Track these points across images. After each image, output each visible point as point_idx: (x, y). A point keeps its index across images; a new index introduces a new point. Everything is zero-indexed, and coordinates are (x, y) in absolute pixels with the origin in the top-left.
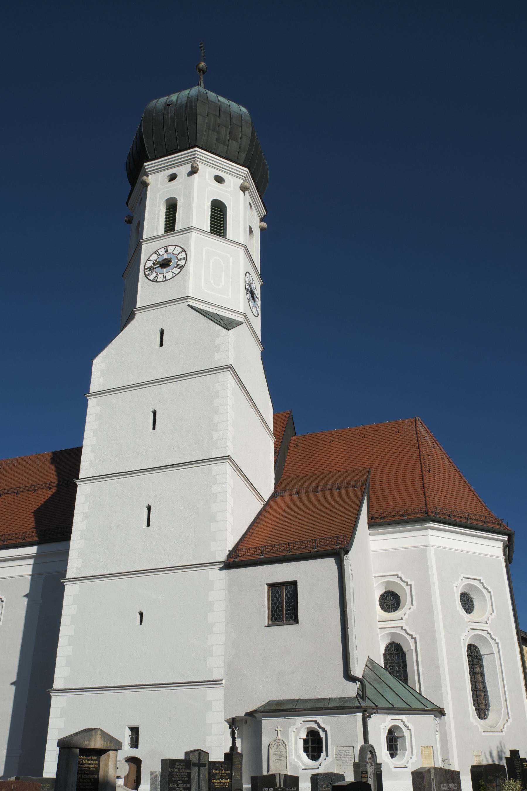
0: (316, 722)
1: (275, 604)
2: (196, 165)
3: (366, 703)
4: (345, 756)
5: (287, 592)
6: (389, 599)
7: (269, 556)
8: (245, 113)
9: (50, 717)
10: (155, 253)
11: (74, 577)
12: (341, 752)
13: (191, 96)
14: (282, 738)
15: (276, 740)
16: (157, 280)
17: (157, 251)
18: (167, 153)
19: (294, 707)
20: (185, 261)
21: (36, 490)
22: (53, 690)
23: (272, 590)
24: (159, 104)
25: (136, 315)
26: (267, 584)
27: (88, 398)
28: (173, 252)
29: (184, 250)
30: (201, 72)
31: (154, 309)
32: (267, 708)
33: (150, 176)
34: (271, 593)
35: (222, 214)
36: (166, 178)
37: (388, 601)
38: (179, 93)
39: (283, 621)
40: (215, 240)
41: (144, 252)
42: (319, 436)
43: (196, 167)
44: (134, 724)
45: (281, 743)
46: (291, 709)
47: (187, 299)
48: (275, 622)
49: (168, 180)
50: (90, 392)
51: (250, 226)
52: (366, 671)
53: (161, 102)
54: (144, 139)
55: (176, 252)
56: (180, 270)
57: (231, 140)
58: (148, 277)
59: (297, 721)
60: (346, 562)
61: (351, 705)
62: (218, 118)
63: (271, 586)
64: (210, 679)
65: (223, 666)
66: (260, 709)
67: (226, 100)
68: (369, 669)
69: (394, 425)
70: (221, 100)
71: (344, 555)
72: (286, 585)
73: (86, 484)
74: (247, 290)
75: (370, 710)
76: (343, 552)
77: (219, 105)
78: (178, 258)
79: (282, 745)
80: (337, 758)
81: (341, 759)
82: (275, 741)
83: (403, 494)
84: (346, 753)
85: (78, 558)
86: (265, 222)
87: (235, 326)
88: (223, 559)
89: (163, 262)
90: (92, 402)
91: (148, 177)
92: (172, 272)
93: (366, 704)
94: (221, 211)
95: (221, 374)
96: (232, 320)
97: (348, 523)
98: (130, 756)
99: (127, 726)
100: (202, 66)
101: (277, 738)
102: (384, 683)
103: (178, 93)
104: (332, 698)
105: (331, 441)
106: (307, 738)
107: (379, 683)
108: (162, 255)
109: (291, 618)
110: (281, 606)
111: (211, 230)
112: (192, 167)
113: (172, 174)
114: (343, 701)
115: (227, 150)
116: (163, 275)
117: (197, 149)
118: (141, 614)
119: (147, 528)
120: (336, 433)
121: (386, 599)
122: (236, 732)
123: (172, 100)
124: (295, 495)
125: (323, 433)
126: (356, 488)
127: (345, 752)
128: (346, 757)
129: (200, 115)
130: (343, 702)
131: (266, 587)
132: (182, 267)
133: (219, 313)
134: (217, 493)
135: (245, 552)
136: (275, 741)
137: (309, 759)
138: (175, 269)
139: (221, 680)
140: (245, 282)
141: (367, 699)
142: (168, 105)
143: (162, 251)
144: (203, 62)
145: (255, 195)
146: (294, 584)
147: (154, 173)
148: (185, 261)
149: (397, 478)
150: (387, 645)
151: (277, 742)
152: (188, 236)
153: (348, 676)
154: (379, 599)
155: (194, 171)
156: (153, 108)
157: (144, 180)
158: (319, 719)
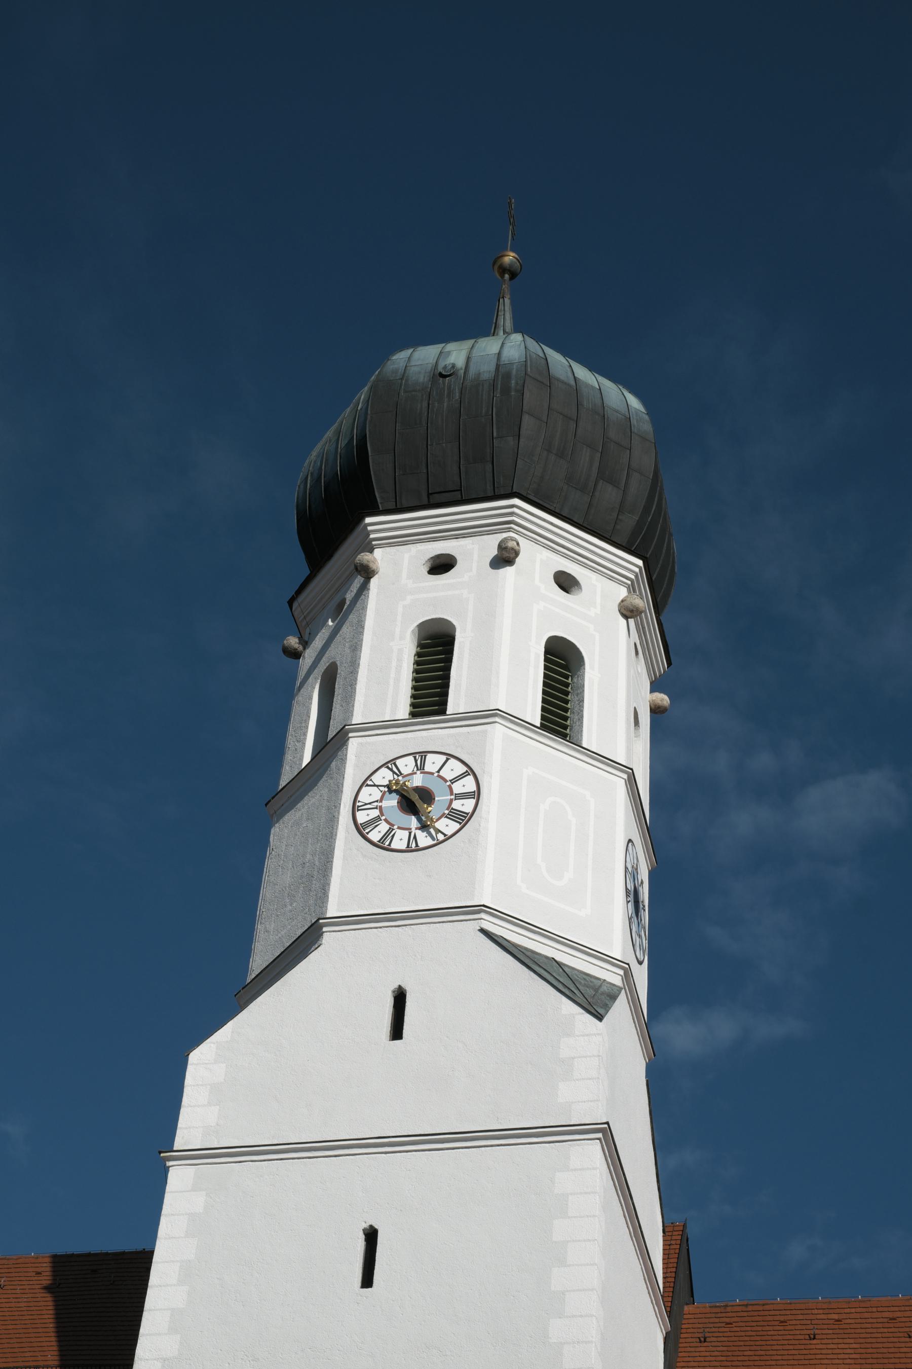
2: (515, 544)
8: (637, 411)
10: (388, 767)
17: (393, 761)
20: (473, 801)
27: (169, 1163)
28: (438, 771)
29: (470, 771)
30: (507, 276)
31: (380, 928)
33: (376, 551)
35: (570, 674)
42: (771, 1313)
43: (513, 549)
50: (175, 1149)
51: (635, 708)
54: (370, 454)
55: (447, 773)
56: (458, 826)
62: (572, 425)
74: (627, 891)
77: (576, 389)
78: (456, 791)
86: (665, 693)
91: (371, 551)
94: (566, 667)
100: (511, 260)
105: (812, 1336)
111: (541, 724)
112: (502, 547)
115: (590, 504)
116: (410, 833)
117: (516, 501)
120: (821, 1311)
123: (453, 366)
132: (463, 820)
138: (444, 821)
140: (626, 868)
143: (407, 765)
144: (513, 250)
148: (473, 801)
149: (779, 1353)
152: (485, 732)
157: (365, 562)
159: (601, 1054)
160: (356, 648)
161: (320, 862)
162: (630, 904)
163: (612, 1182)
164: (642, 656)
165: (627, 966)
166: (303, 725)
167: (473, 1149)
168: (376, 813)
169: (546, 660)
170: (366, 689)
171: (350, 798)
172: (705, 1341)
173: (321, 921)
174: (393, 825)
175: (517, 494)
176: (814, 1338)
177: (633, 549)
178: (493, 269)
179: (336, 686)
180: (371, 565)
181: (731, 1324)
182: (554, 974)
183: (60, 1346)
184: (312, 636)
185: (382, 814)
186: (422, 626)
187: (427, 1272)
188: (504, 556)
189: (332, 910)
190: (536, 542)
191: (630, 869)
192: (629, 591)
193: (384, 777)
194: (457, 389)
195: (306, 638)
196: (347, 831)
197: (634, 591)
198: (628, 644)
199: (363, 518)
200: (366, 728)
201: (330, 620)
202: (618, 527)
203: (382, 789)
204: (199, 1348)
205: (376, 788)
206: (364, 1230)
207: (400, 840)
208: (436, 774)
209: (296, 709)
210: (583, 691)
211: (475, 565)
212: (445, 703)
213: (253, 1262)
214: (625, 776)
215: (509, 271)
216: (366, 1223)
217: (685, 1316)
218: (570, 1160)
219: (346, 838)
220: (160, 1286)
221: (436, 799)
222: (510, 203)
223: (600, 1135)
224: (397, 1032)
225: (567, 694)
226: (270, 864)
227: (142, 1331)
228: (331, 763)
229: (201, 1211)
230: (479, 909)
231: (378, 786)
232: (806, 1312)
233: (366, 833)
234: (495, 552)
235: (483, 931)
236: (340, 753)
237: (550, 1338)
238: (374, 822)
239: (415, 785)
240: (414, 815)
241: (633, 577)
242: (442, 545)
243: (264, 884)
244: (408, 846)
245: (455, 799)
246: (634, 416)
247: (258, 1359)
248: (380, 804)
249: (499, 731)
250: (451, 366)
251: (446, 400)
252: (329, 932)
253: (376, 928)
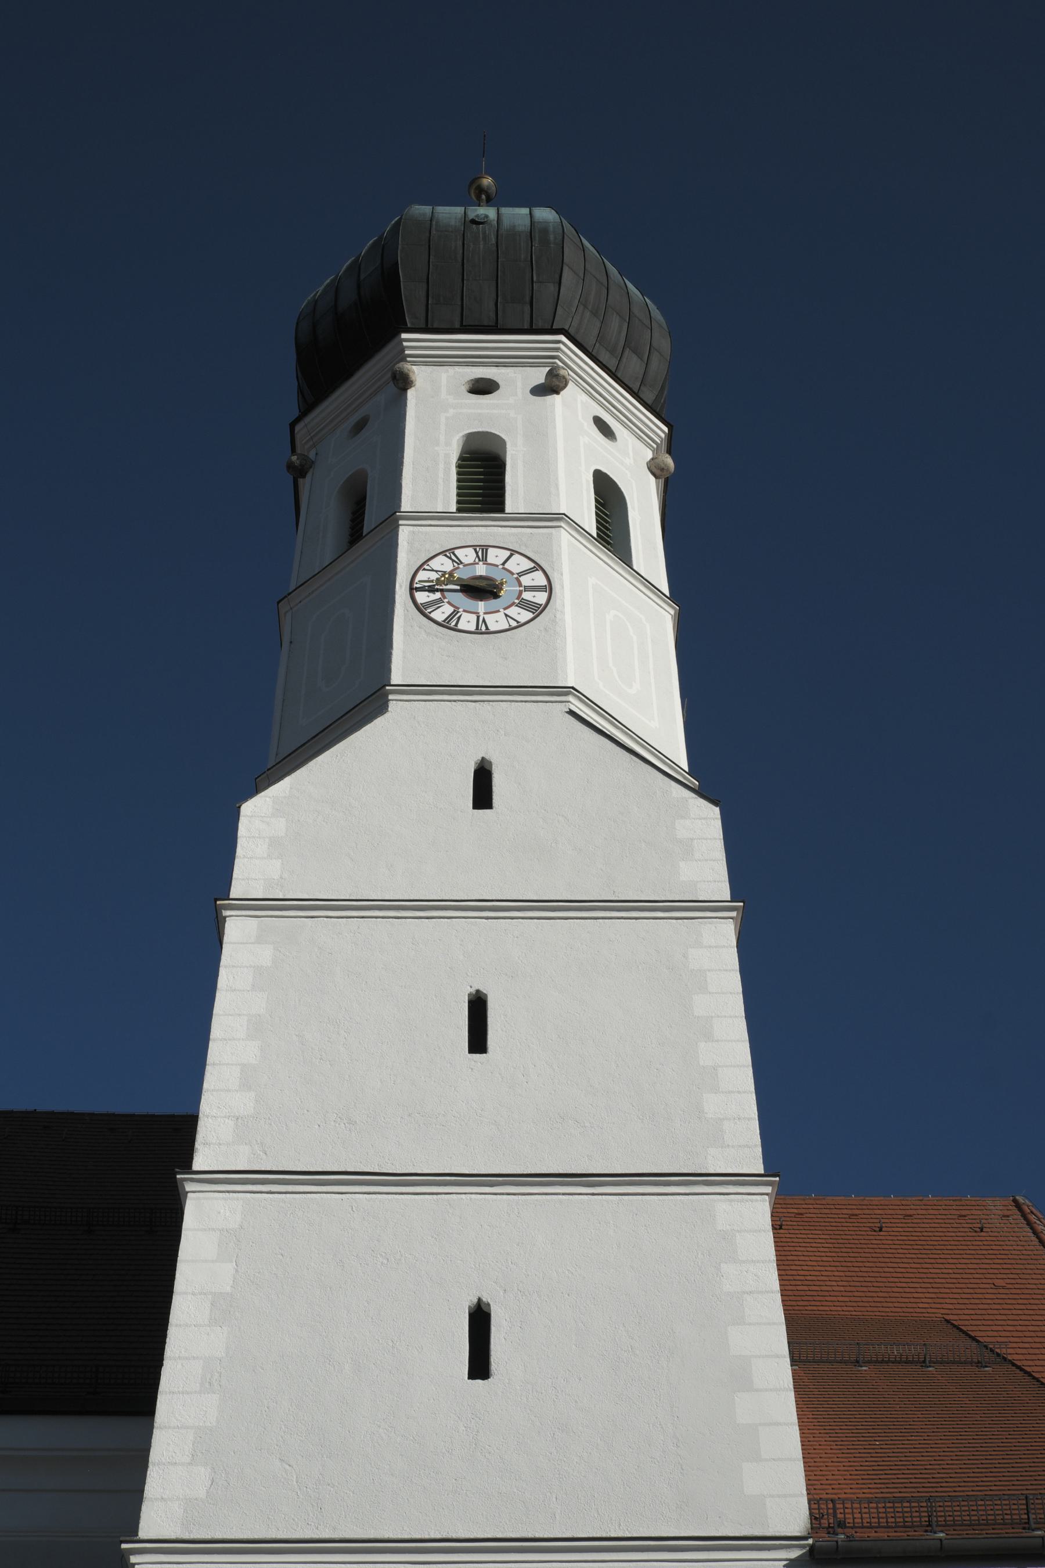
10: (475, 550)
16: (430, 613)
25: (391, 704)
27: (226, 913)
31: (455, 701)
36: (464, 383)
41: (405, 543)
50: (231, 896)
56: (530, 615)
78: (524, 583)
85: (190, 1464)
88: (797, 1528)
89: (472, 583)
92: (506, 615)
134: (744, 1293)
143: (467, 556)
155: (552, 386)
167: (589, 920)
170: (412, 485)
171: (407, 580)
174: (458, 608)
175: (564, 331)
178: (469, 193)
180: (411, 374)
186: (470, 438)
187: (552, 1040)
188: (553, 384)
200: (417, 516)
204: (280, 1107)
208: (501, 567)
213: (338, 1020)
214: (672, 612)
216: (471, 987)
218: (702, 937)
220: (225, 1040)
229: (269, 965)
230: (567, 691)
233: (429, 612)
235: (571, 713)
237: (706, 1113)
242: (481, 370)
245: (525, 591)
247: (356, 1122)
249: (564, 537)
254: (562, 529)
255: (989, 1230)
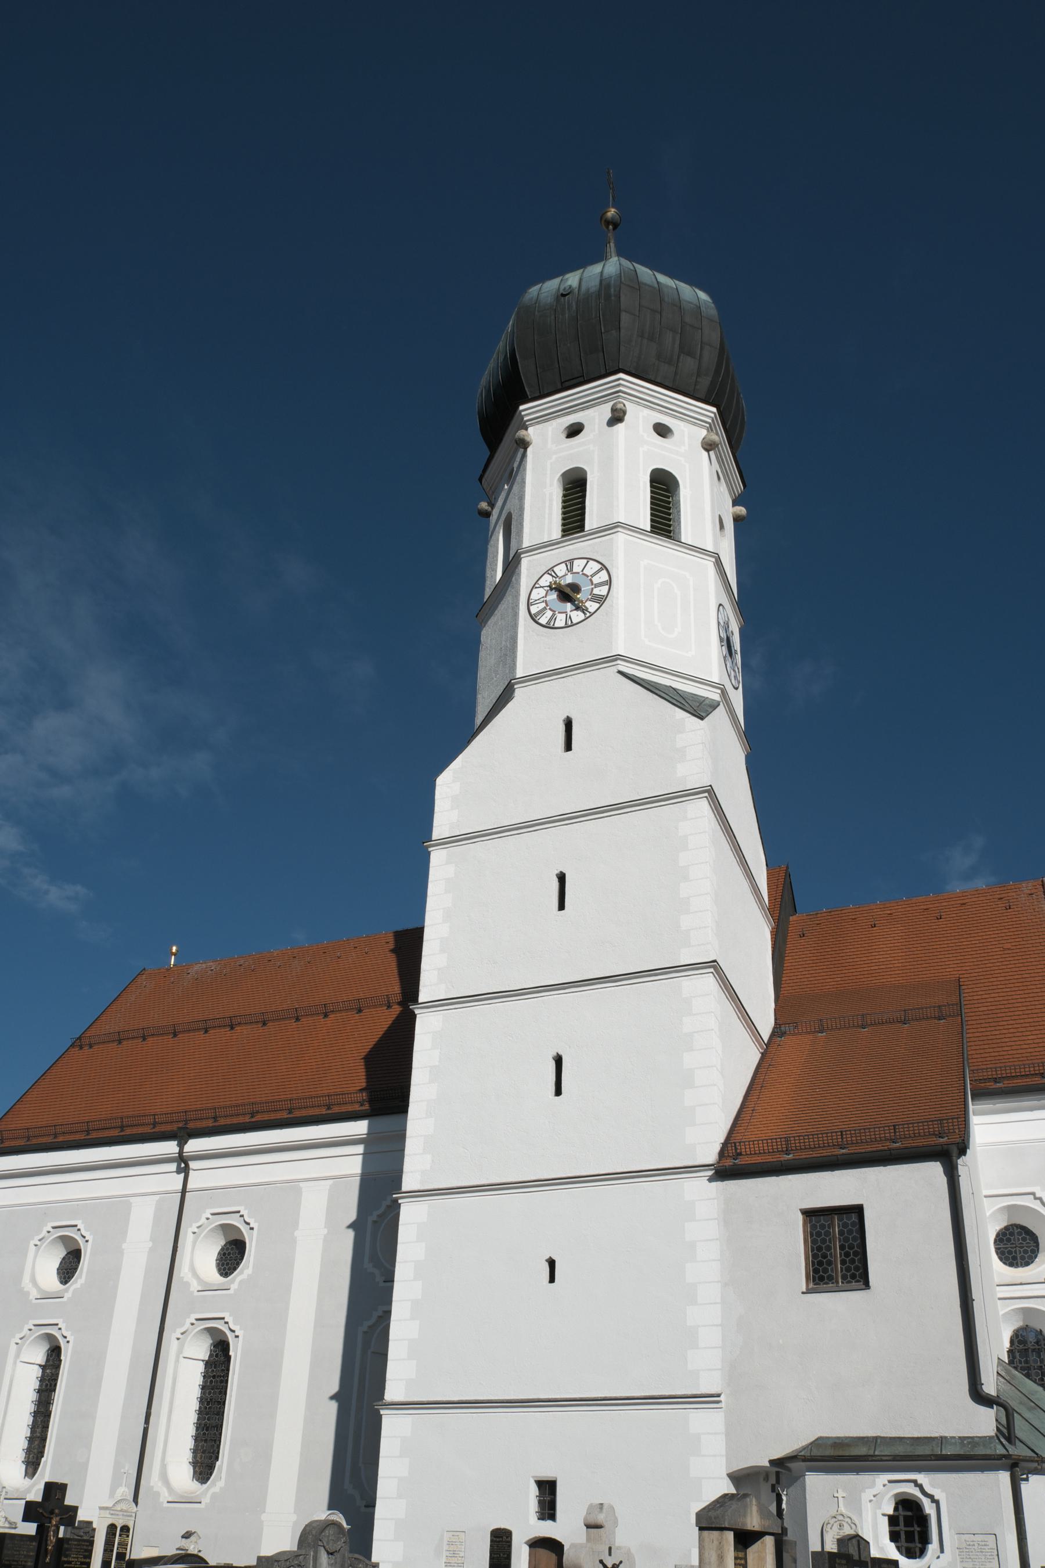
0: (915, 1482)
1: (819, 1249)
2: (622, 405)
3: (1016, 1448)
4: (978, 1552)
5: (843, 1227)
6: (1015, 1241)
7: (804, 1155)
9: (381, 1454)
10: (549, 574)
11: (416, 1188)
12: (969, 1545)
13: (607, 277)
14: (848, 1513)
15: (837, 1515)
16: (554, 625)
17: (552, 569)
18: (562, 385)
19: (871, 1453)
20: (607, 587)
21: (300, 1018)
22: (385, 1403)
23: (811, 1221)
24: (545, 294)
26: (801, 1210)
28: (582, 571)
29: (604, 567)
31: (552, 680)
32: (816, 1452)
33: (529, 429)
34: (811, 1229)
37: (1013, 1244)
38: (584, 271)
39: (837, 1282)
40: (659, 547)
41: (525, 571)
43: (621, 409)
44: (546, 1474)
45: (847, 1522)
46: (865, 1456)
47: (616, 660)
48: (820, 1284)
49: (566, 436)
50: (433, 839)
51: (720, 516)
52: (1000, 1384)
53: (547, 290)
54: (518, 360)
55: (588, 571)
56: (598, 605)
57: (682, 355)
58: (537, 619)
59: (876, 1480)
60: (962, 1170)
61: (988, 1452)
62: (658, 316)
63: (809, 1214)
64: (695, 1392)
65: (720, 1367)
66: (802, 1453)
67: (669, 279)
68: (1005, 1381)
69: (998, 893)
70: (662, 281)
71: (959, 1158)
72: (839, 1214)
73: (435, 1013)
75: (1022, 1464)
76: (955, 1151)
77: (659, 291)
78: (595, 582)
79: (849, 1527)
80: (962, 1557)
81: (970, 1558)
82: (835, 1517)
83: (1034, 1033)
84: (980, 1547)
86: (743, 506)
87: (710, 711)
90: (437, 858)
91: (526, 429)
93: (1017, 1451)
94: (667, 491)
95: (690, 803)
96: (700, 698)
97: (947, 1091)
98: (541, 1535)
99: (533, 1477)
100: (613, 214)
101: (837, 1511)
102: (1039, 1410)
103: (580, 271)
104: (946, 1437)
105: (873, 926)
106: (897, 1513)
107: (1030, 1409)
108: (561, 577)
109: (853, 1277)
110: (831, 1254)
111: (652, 526)
112: (614, 410)
113: (574, 424)
114: (969, 1443)
115: (676, 373)
116: (567, 615)
117: (621, 375)
118: (552, 1263)
119: (556, 1097)
121: (1009, 1240)
122: (784, 1498)
123: (570, 286)
124: (820, 1032)
125: (853, 910)
126: (942, 1020)
127: (979, 1544)
128: (981, 1554)
129: (625, 311)
130: (970, 1446)
131: (800, 1217)
132: (602, 598)
133: (675, 685)
135: (762, 1149)
136: (835, 1517)
137: (902, 1555)
139: (719, 1396)
140: (719, 623)
141: (1017, 1441)
142: (563, 295)
143: (561, 570)
144: (613, 207)
145: (726, 458)
146: (858, 1211)
147: (538, 423)
150: (1014, 1331)
151: (838, 1520)
153: (978, 1396)
154: (995, 1241)
155: (617, 417)
156: (533, 303)
157: (522, 437)
158: (922, 1478)
159: (704, 742)
160: (521, 498)
161: (510, 644)
162: (723, 647)
163: (719, 827)
164: (723, 481)
165: (722, 687)
166: (495, 559)
168: (543, 605)
169: (652, 486)
172: (804, 936)
173: (512, 681)
174: (555, 612)
176: (875, 927)
177: (711, 401)
179: (512, 527)
180: (526, 438)
181: (820, 924)
182: (670, 695)
183: (400, 979)
184: (496, 499)
185: (547, 605)
186: (565, 475)
188: (616, 416)
189: (519, 673)
190: (638, 404)
191: (722, 624)
192: (708, 431)
193: (547, 580)
194: (574, 303)
195: (493, 502)
196: (525, 620)
197: (712, 430)
198: (710, 470)
199: (518, 407)
200: (531, 550)
201: (506, 485)
202: (698, 387)
203: (546, 588)
205: (542, 589)
206: (557, 875)
207: (560, 621)
209: (490, 549)
210: (680, 505)
211: (597, 426)
212: (583, 520)
214: (713, 560)
215: (612, 222)
217: (791, 923)
219: (525, 625)
221: (582, 589)
222: (608, 172)
223: (706, 794)
224: (568, 747)
225: (669, 509)
226: (482, 654)
227: (423, 953)
228: (512, 578)
231: (543, 587)
232: (869, 911)
234: (610, 415)
235: (620, 672)
236: (517, 570)
238: (542, 612)
239: (567, 582)
240: (569, 602)
241: (710, 421)
243: (480, 668)
244: (566, 624)
246: (704, 306)
248: (545, 599)
249: (621, 538)
250: (568, 287)
251: (567, 312)
252: (519, 688)
253: (549, 681)
254: (619, 533)
255: (1015, 907)
